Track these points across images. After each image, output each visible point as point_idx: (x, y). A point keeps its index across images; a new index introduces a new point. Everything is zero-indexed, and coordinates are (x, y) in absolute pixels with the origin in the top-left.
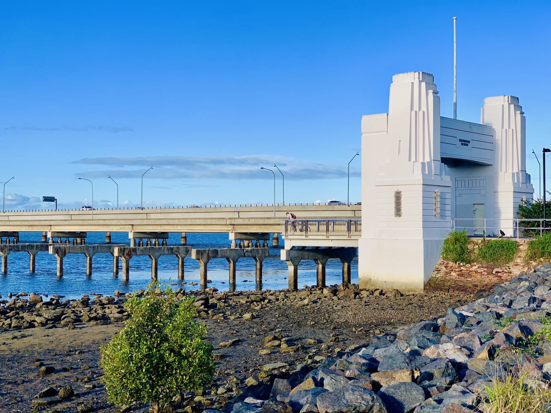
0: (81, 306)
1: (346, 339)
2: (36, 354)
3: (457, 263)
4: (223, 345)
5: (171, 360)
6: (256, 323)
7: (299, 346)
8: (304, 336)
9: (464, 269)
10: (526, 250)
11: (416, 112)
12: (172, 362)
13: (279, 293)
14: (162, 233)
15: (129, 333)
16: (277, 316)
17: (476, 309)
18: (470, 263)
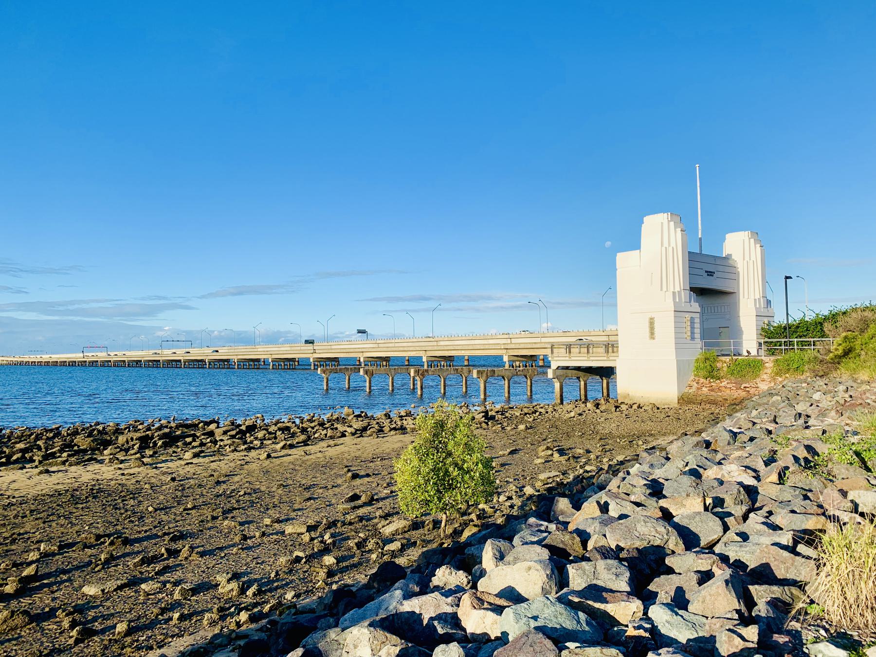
0: (384, 417)
2: (345, 461)
3: (708, 379)
11: (666, 248)
12: (456, 476)
16: (548, 427)
18: (719, 379)
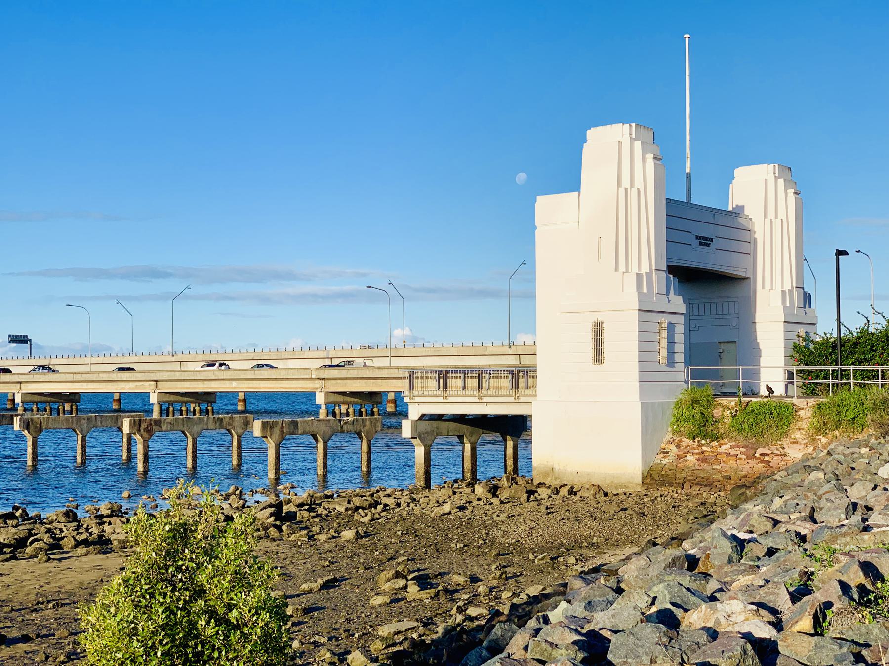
0: (63, 519)
1: (518, 574)
3: (696, 440)
4: (307, 588)
5: (210, 632)
7: (439, 588)
8: (446, 569)
9: (707, 450)
10: (810, 418)
11: (626, 190)
12: (211, 637)
13: (400, 493)
15: (131, 582)
16: (399, 533)
17: (755, 525)
18: (716, 439)
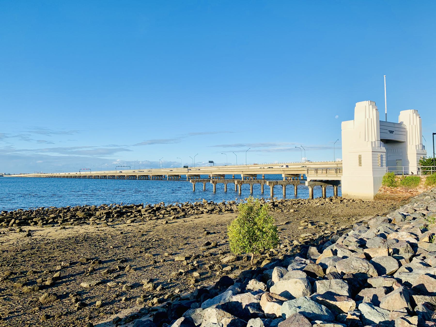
0: (222, 205)
3: (390, 187)
6: (296, 214)
8: (319, 221)
11: (368, 119)
14: (254, 174)
16: (305, 211)
